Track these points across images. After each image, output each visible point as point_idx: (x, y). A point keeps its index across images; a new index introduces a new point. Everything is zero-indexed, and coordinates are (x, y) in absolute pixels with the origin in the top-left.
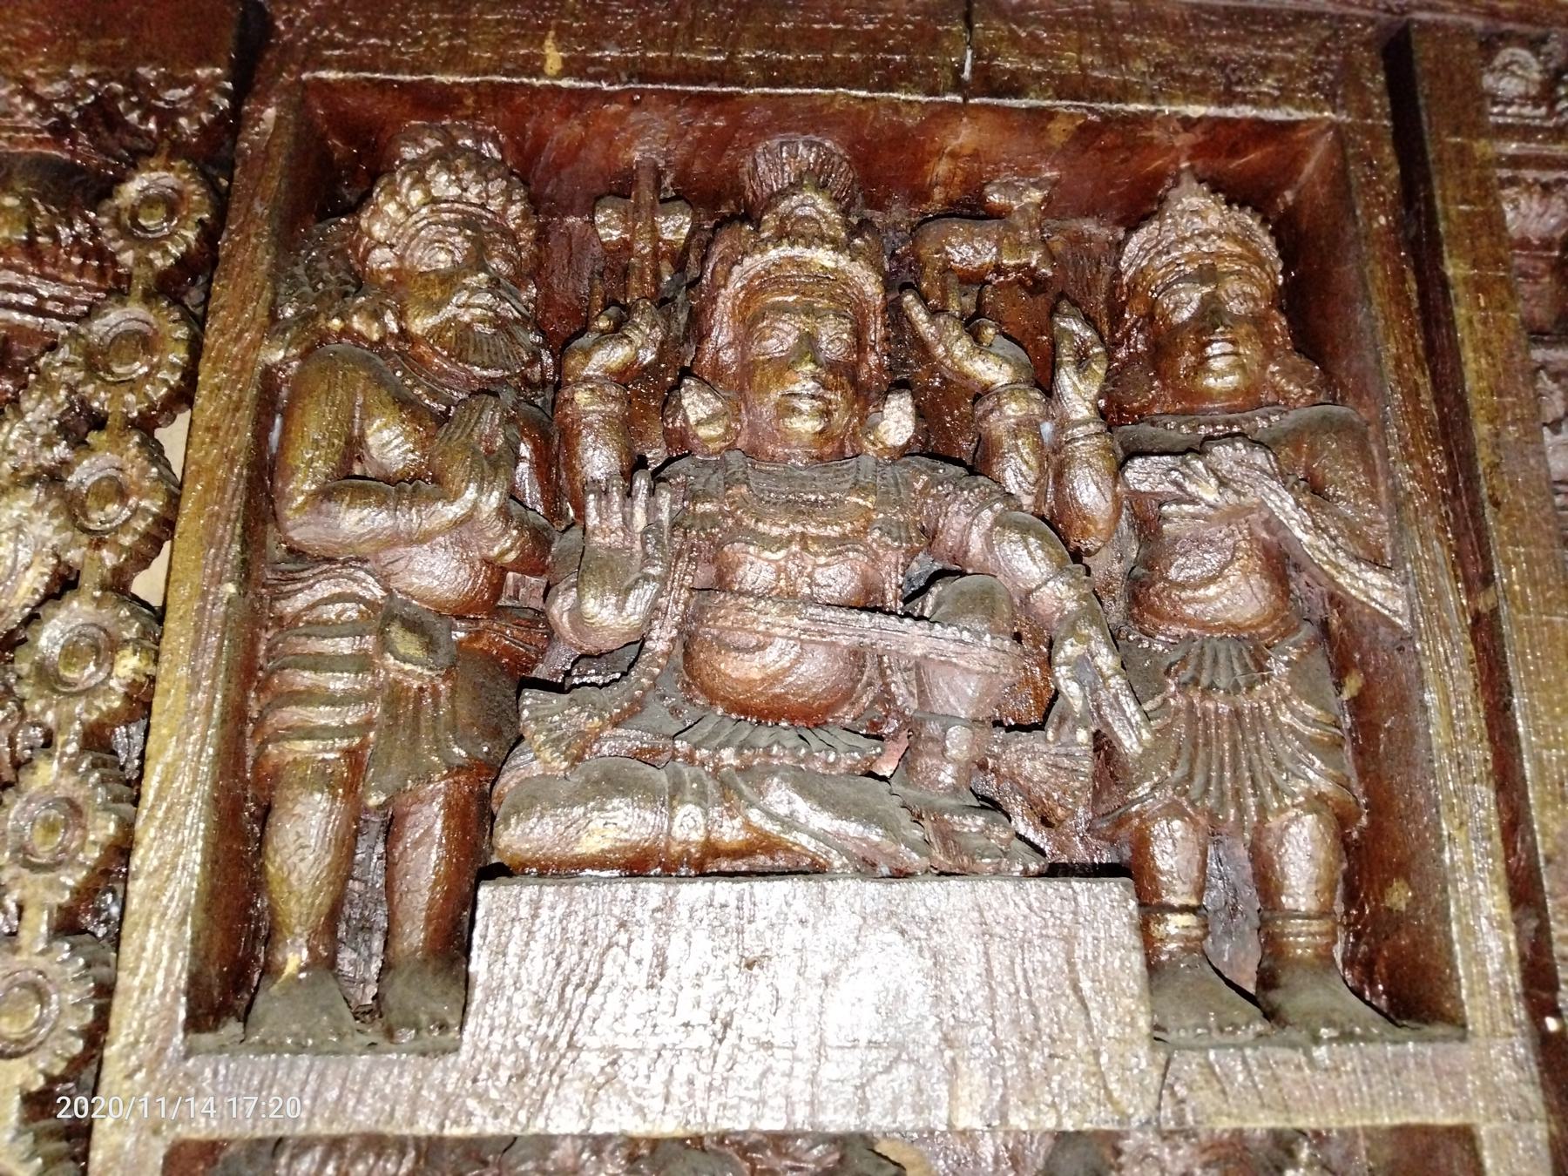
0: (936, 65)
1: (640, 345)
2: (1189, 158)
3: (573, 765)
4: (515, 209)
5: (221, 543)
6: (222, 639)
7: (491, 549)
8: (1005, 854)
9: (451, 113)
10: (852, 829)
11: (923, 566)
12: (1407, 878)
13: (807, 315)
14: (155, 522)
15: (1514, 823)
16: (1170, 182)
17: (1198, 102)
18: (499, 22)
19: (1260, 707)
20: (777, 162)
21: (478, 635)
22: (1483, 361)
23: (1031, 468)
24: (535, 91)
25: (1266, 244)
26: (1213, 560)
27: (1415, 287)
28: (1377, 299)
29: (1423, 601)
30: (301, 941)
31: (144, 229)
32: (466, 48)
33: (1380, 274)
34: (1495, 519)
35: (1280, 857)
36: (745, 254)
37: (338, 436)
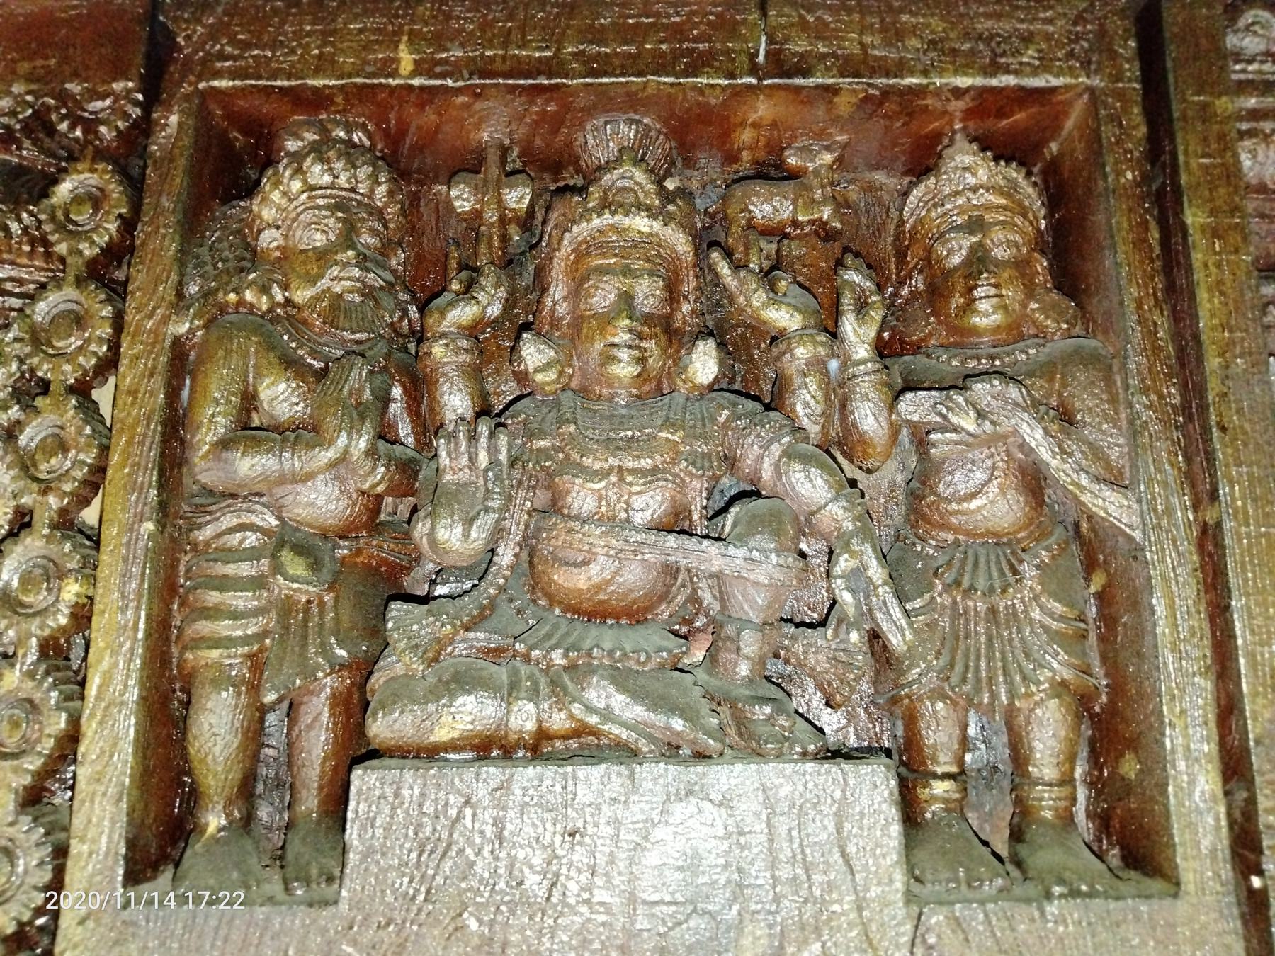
0: (734, 51)
1: (490, 301)
2: (961, 121)
3: (429, 665)
4: (382, 190)
5: (141, 489)
6: (144, 568)
7: (363, 483)
8: (787, 739)
9: (326, 109)
10: (659, 719)
11: (729, 485)
12: (1137, 752)
13: (624, 276)
14: (90, 472)
15: (1228, 710)
16: (946, 141)
17: (966, 74)
18: (361, 31)
19: (1014, 605)
20: (604, 138)
21: (359, 551)
22: (1216, 301)
23: (818, 402)
24: (392, 90)
25: (1030, 193)
26: (979, 476)
27: (1157, 236)
28: (1121, 248)
29: (1156, 519)
30: (220, 807)
31: (76, 224)
32: (334, 54)
33: (1126, 226)
34: (1222, 440)
35: (1028, 733)
36: (574, 222)
37: (234, 394)
